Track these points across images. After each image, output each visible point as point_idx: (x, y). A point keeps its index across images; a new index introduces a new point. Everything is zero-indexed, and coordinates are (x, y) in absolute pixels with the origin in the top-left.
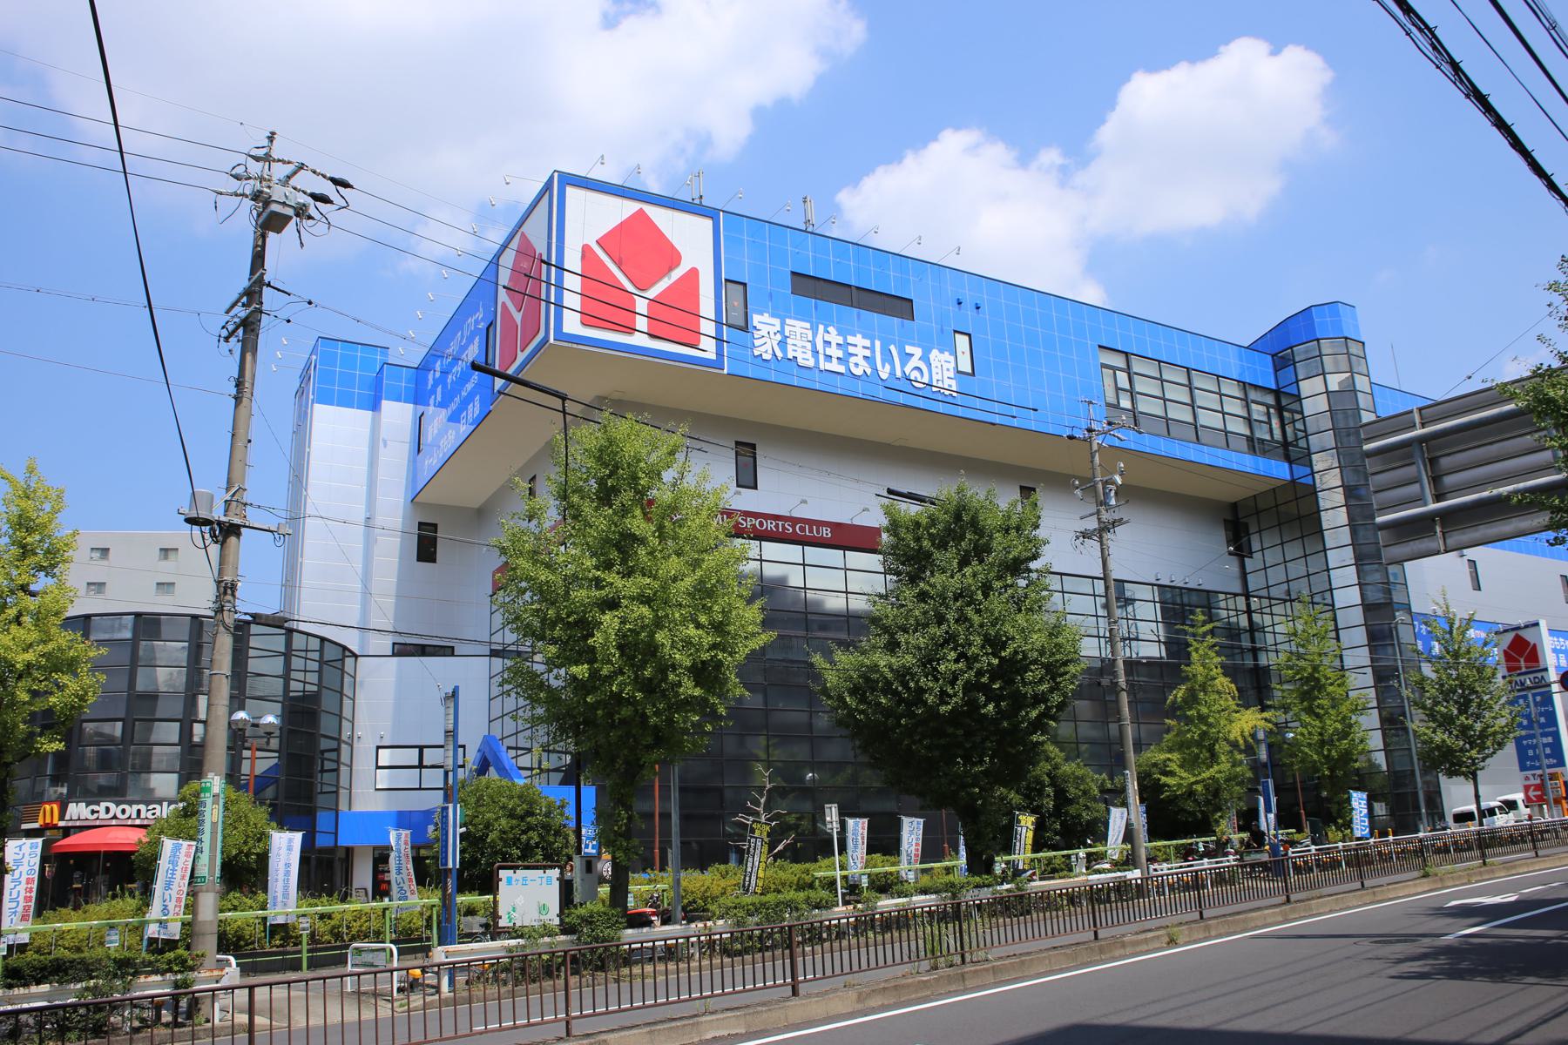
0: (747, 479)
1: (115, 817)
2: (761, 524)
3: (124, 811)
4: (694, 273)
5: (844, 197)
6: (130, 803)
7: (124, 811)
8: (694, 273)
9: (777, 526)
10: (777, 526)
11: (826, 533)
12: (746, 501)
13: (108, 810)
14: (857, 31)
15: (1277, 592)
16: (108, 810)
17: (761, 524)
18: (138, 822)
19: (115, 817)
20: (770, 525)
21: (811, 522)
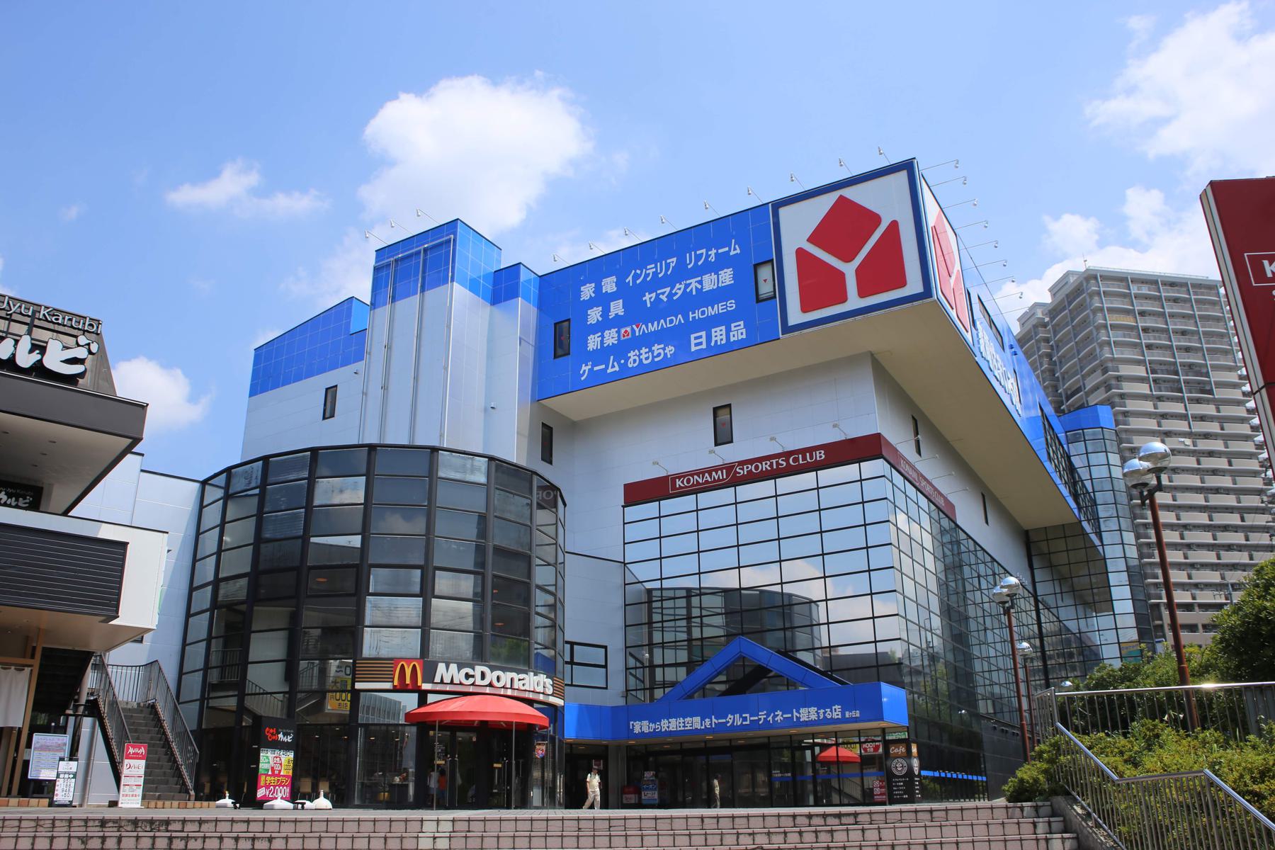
0: (723, 436)
1: (491, 685)
2: (757, 468)
3: (498, 679)
4: (894, 226)
5: (1131, 193)
6: (493, 669)
7: (498, 679)
8: (894, 226)
9: (771, 465)
10: (771, 465)
11: (819, 456)
12: (729, 454)
13: (483, 676)
14: (556, 92)
15: (987, 682)
16: (483, 676)
17: (757, 468)
18: (509, 692)
19: (491, 685)
20: (765, 466)
21: (803, 451)
